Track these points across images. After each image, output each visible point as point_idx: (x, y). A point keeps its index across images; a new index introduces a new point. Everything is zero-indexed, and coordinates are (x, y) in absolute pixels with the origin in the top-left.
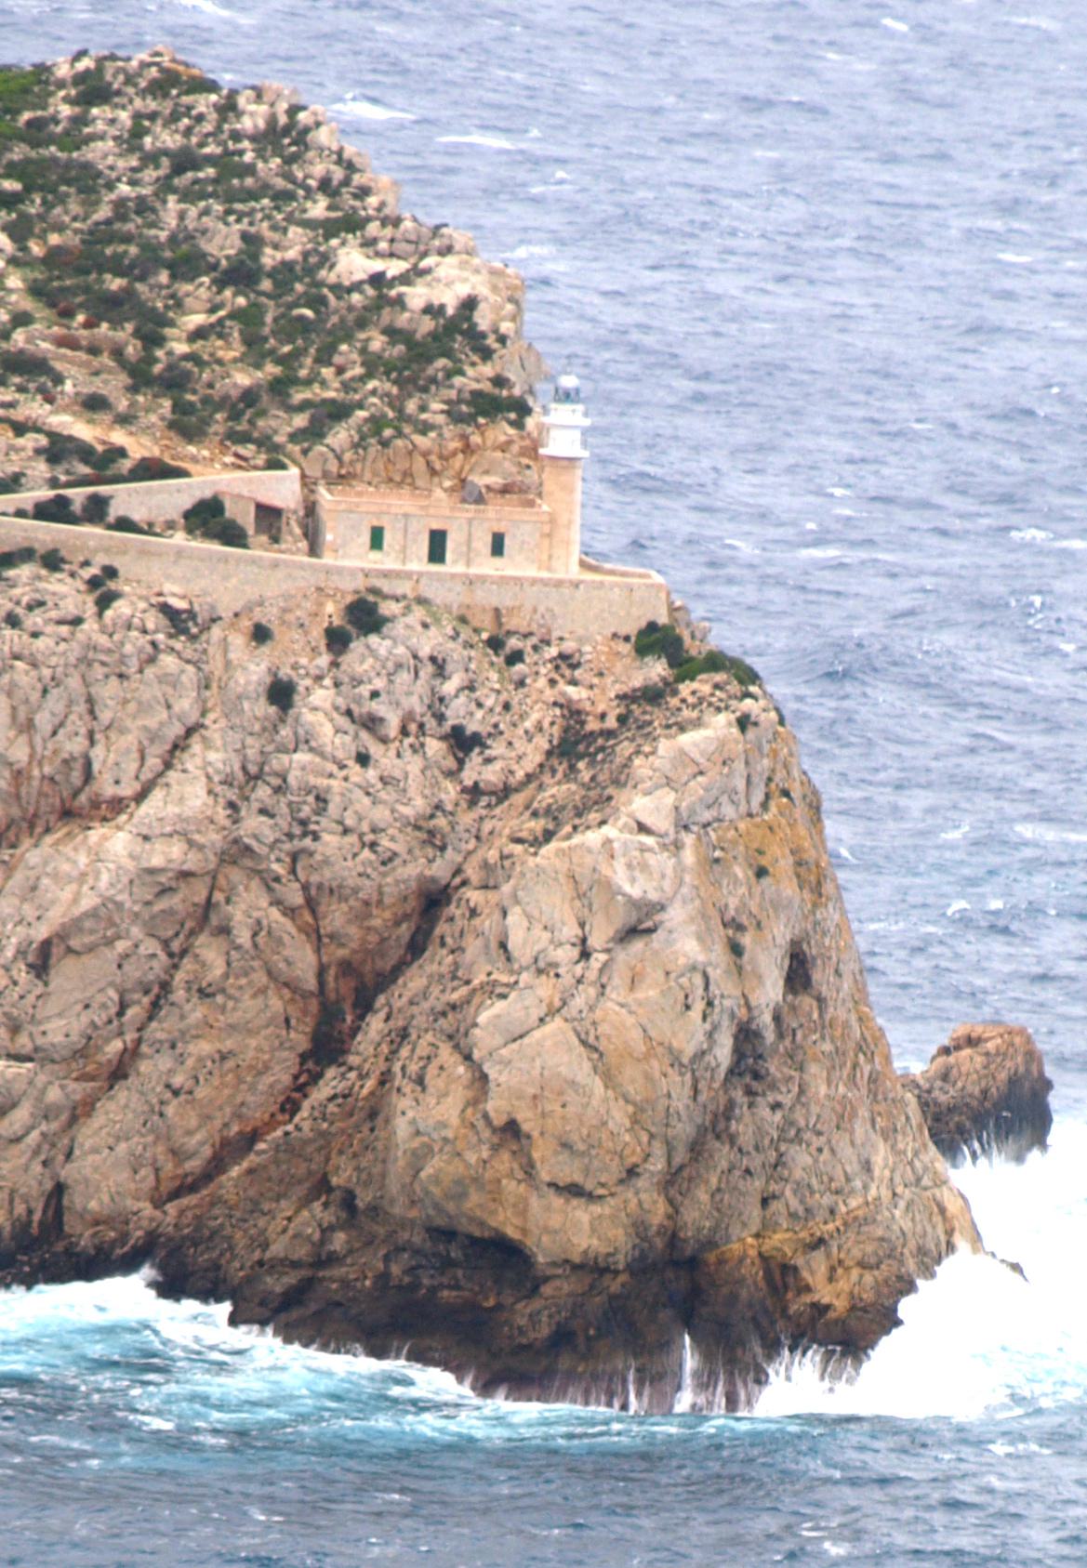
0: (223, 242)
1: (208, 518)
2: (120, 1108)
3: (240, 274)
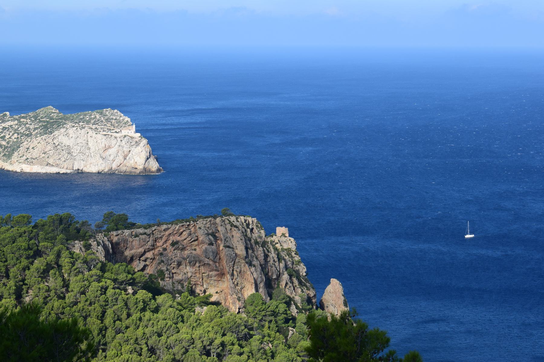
0: (114, 118)
1: (116, 132)
2: (114, 162)
3: (116, 119)
